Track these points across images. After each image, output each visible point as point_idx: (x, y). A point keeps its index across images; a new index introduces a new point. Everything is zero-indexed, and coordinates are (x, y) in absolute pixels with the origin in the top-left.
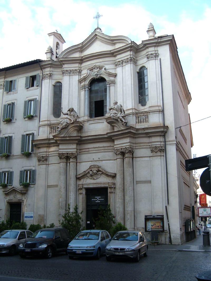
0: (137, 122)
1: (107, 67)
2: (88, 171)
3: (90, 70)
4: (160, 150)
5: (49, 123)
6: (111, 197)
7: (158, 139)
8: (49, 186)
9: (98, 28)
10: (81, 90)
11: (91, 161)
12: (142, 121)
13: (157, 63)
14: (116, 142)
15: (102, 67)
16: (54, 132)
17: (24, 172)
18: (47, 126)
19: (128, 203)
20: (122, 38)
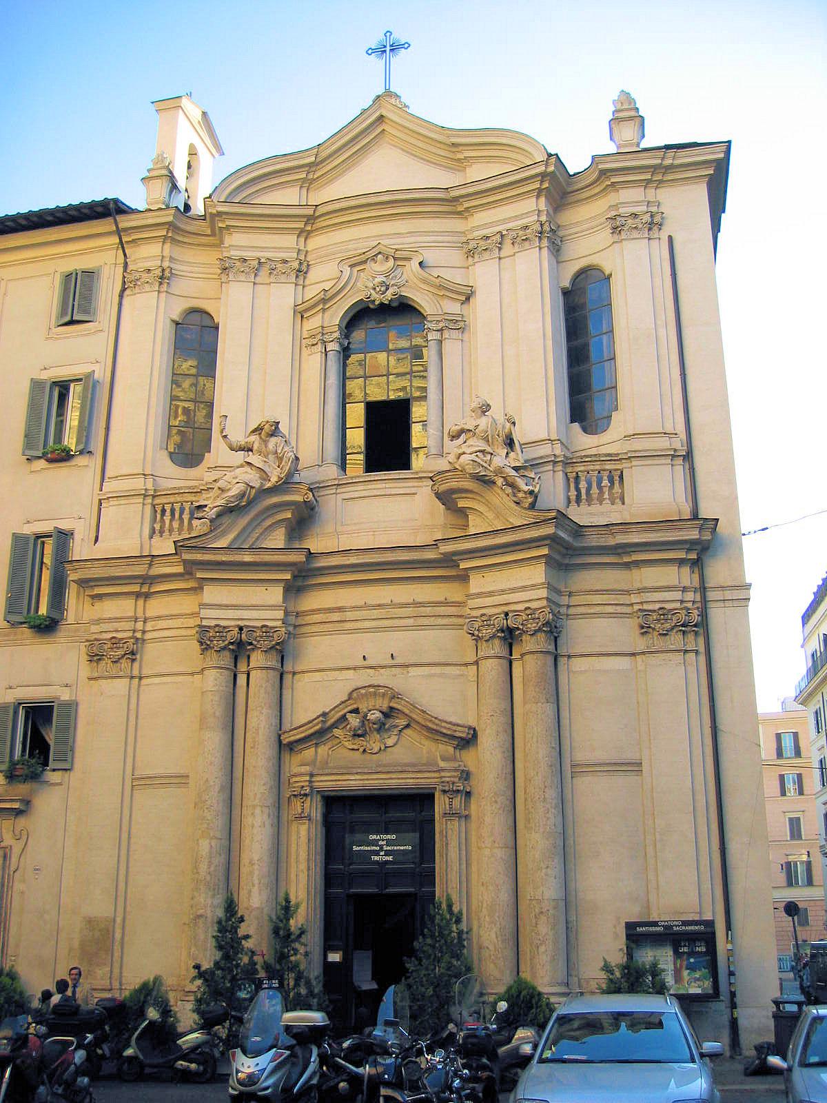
0: (573, 498)
1: (430, 256)
3: (351, 266)
4: (683, 625)
5: (150, 485)
6: (447, 833)
7: (670, 575)
8: (141, 782)
9: (389, 94)
10: (305, 352)
11: (354, 669)
12: (595, 496)
13: (656, 253)
14: (477, 583)
15: (405, 254)
16: (171, 530)
17: (16, 713)
20: (504, 141)
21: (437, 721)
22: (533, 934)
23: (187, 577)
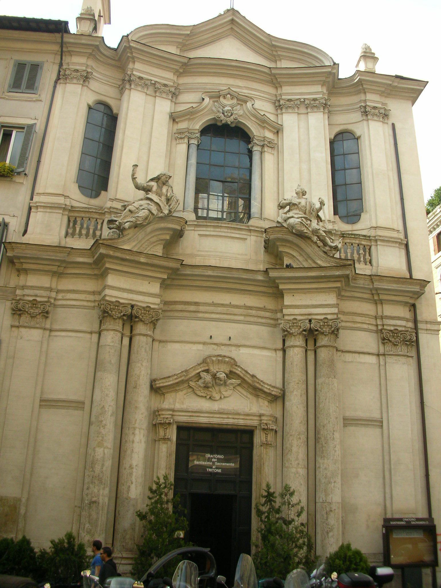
2: (197, 371)
16: (80, 234)
18: (61, 211)
19: (332, 480)
21: (262, 383)
22: (324, 524)
23: (94, 266)
